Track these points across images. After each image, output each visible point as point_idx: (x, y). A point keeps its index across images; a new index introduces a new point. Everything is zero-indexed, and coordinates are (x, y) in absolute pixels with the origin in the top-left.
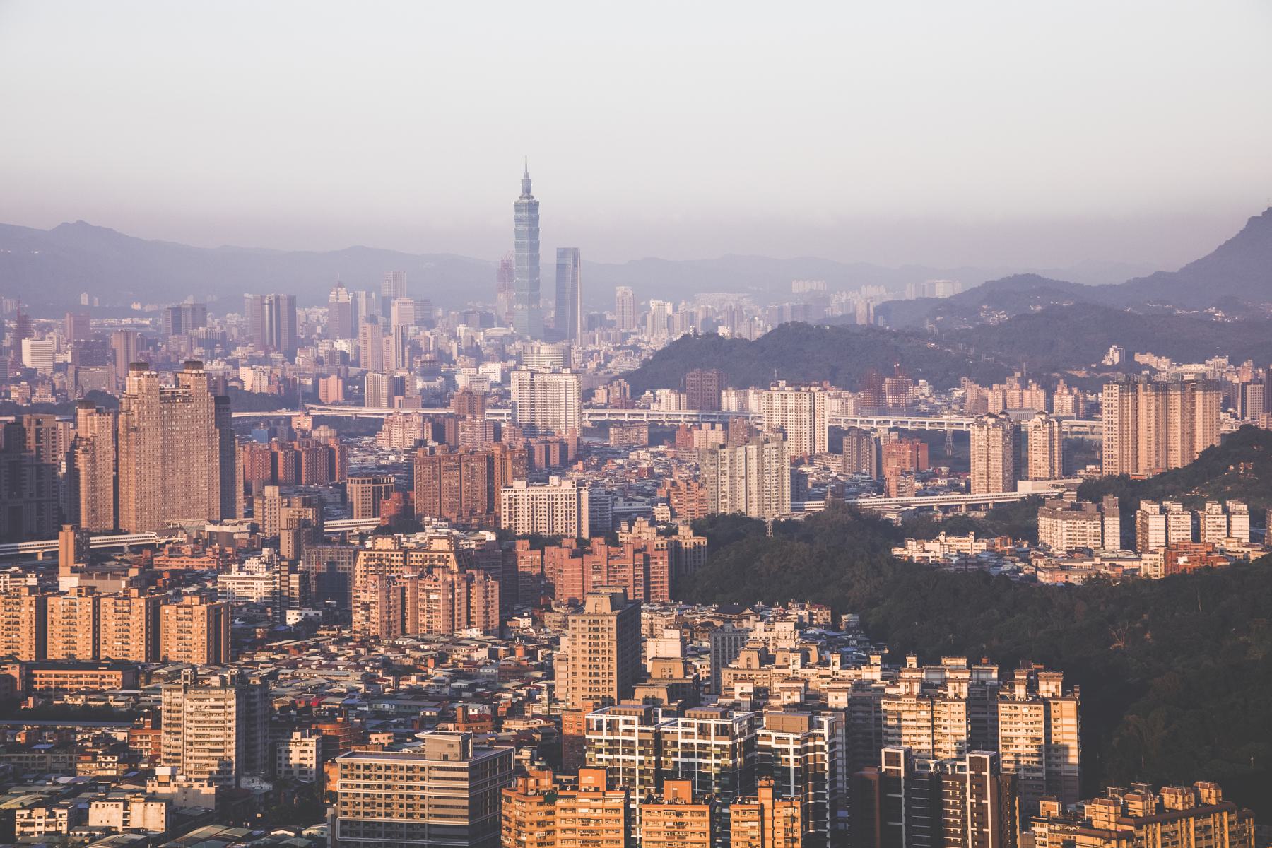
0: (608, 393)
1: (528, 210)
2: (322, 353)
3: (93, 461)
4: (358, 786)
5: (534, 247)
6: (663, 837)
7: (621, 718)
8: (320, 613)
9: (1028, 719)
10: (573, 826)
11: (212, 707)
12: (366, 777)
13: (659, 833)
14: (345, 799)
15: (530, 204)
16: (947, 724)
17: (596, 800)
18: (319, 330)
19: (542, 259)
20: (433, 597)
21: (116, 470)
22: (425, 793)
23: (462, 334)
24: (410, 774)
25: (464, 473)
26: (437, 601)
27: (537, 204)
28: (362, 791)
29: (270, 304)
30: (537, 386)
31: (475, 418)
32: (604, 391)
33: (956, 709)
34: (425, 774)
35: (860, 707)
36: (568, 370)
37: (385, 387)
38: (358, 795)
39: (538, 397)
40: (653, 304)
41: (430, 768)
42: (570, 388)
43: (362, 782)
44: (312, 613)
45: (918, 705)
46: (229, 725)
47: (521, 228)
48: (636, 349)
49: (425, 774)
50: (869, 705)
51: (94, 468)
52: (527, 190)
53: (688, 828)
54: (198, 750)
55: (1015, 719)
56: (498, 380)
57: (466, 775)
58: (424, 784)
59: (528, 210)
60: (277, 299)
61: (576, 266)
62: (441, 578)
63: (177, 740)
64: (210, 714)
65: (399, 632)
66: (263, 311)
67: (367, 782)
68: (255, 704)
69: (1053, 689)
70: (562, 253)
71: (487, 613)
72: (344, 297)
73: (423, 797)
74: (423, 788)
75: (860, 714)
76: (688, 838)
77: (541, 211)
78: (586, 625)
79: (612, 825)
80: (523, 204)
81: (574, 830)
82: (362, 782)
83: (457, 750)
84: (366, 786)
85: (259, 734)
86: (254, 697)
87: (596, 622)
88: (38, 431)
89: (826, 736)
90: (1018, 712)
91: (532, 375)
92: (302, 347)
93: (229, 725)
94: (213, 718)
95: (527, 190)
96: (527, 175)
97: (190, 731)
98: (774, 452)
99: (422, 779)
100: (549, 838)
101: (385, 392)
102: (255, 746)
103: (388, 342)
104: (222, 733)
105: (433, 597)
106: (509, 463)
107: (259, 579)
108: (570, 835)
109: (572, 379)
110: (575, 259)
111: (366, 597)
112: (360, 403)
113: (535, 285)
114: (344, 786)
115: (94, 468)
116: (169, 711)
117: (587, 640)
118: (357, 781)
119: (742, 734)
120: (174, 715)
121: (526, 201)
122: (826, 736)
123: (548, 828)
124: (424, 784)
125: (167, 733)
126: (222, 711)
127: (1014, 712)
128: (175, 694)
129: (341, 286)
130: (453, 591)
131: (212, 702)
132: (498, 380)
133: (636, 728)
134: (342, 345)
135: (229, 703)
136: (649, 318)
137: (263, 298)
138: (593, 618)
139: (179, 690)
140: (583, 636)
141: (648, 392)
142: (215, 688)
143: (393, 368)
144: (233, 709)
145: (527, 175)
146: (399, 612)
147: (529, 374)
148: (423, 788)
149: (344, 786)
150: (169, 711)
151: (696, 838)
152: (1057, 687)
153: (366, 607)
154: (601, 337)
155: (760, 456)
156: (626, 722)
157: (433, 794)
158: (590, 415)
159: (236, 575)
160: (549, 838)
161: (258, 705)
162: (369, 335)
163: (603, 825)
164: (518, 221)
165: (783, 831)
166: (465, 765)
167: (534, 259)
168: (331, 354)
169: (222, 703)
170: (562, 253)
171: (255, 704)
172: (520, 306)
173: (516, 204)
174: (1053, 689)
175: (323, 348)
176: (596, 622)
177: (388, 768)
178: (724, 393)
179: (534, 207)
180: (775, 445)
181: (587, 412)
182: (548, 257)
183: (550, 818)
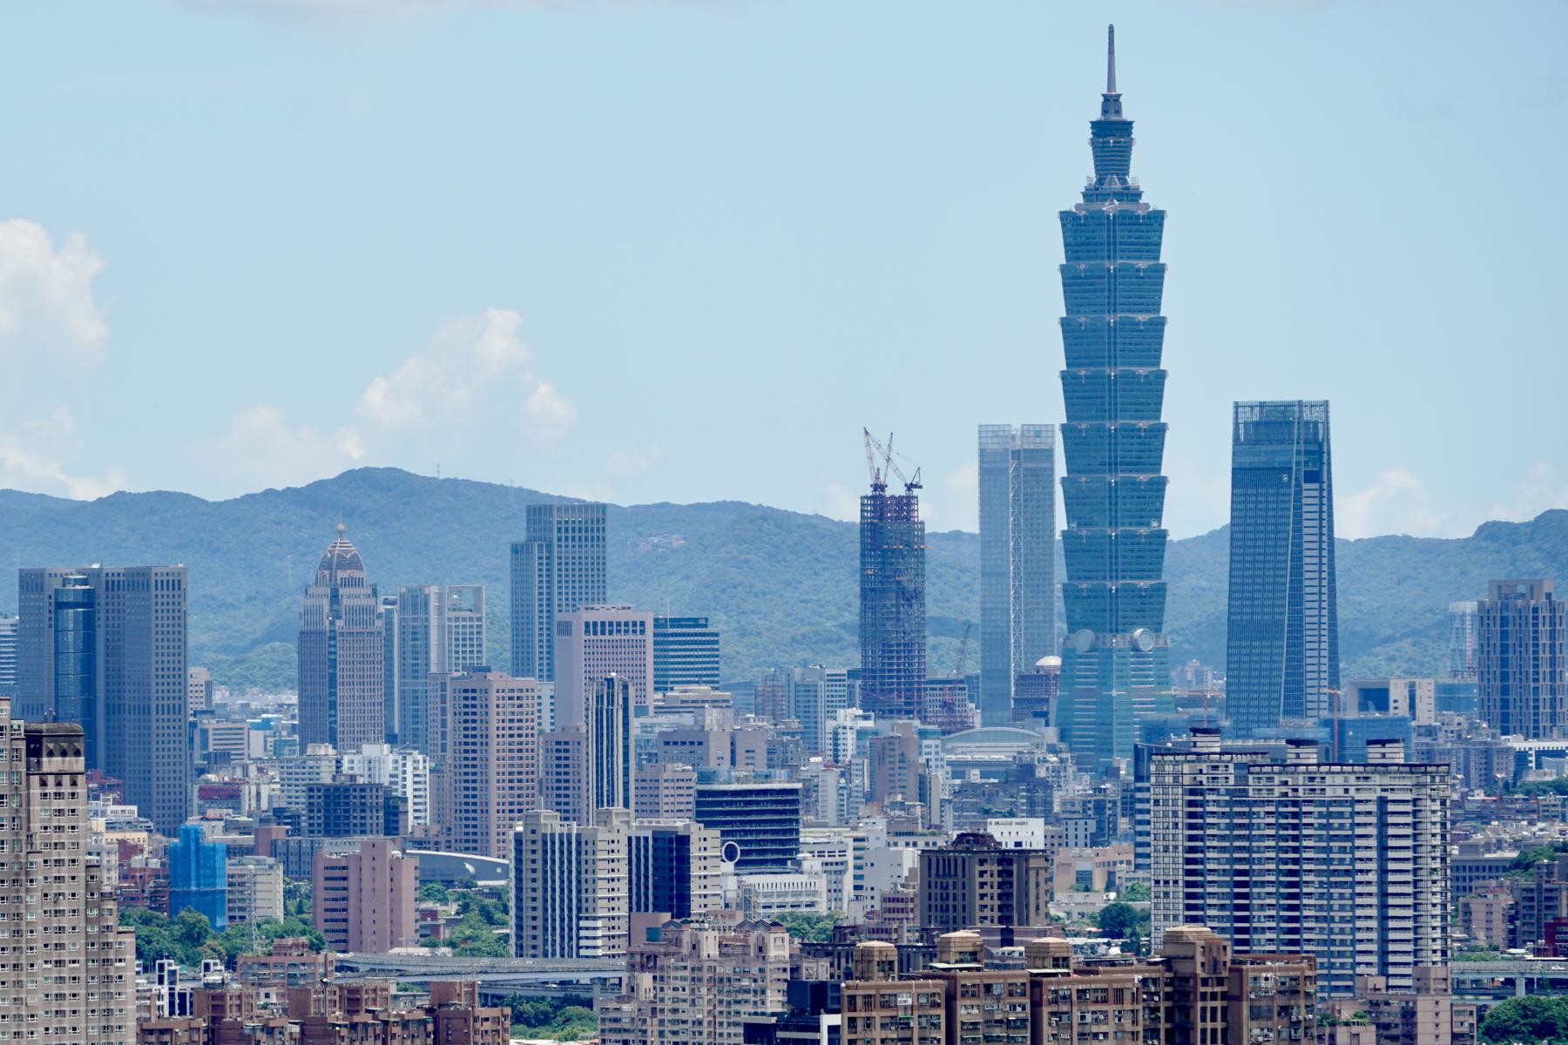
52: (1112, 136)
95: (1112, 136)
96: (1111, 102)
145: (1111, 102)
182: (1197, 496)
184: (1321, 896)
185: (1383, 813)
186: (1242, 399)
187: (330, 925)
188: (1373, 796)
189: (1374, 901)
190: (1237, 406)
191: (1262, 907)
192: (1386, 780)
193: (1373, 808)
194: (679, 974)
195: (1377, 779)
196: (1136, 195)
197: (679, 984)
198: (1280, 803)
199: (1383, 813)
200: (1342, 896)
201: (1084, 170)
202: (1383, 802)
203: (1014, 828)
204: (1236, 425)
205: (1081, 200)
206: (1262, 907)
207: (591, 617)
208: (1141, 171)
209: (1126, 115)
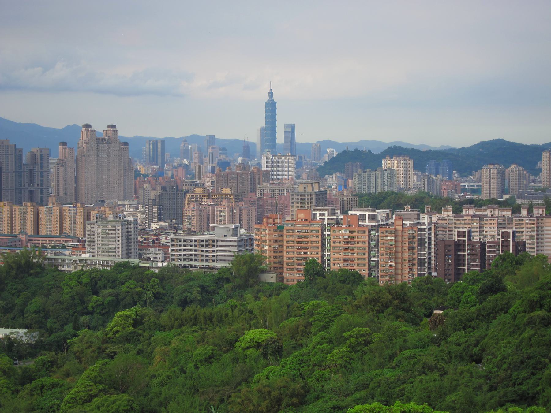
1: (271, 107)
3: (66, 170)
4: (180, 250)
6: (342, 245)
7: (318, 212)
8: (167, 224)
9: (529, 226)
10: (292, 250)
11: (110, 230)
12: (184, 246)
13: (340, 242)
14: (173, 257)
16: (487, 229)
17: (306, 225)
19: (277, 124)
20: (222, 214)
21: (76, 182)
22: (215, 254)
24: (207, 244)
25: (239, 181)
26: (224, 216)
27: (276, 103)
28: (182, 253)
29: (153, 144)
30: (275, 162)
33: (492, 222)
34: (215, 244)
35: (442, 229)
38: (180, 255)
41: (217, 241)
42: (290, 163)
43: (182, 248)
44: (163, 224)
45: (472, 220)
46: (118, 239)
49: (215, 244)
50: (445, 228)
51: (66, 174)
52: (271, 94)
53: (356, 239)
54: (103, 252)
55: (522, 226)
57: (236, 244)
58: (215, 249)
59: (271, 107)
62: (226, 205)
63: (93, 249)
64: (110, 234)
65: (205, 229)
67: (185, 248)
68: (131, 232)
69: (540, 212)
70: (287, 126)
71: (249, 223)
73: (214, 256)
74: (213, 251)
75: (441, 232)
76: (356, 245)
77: (277, 106)
78: (299, 197)
79: (314, 239)
81: (293, 252)
82: (182, 248)
83: (232, 232)
84: (185, 250)
85: (133, 247)
86: (130, 228)
87: (304, 195)
88: (41, 155)
89: (427, 223)
90: (523, 222)
91: (272, 157)
93: (118, 239)
94: (110, 236)
95: (271, 94)
96: (271, 90)
97: (98, 242)
98: (389, 175)
99: (214, 246)
100: (280, 249)
102: (131, 239)
104: (114, 243)
105: (222, 214)
106: (261, 176)
107: (140, 212)
108: (291, 244)
111: (189, 214)
114: (173, 250)
115: (66, 174)
116: (89, 235)
117: (299, 205)
118: (180, 248)
119: (382, 220)
120: (91, 237)
122: (427, 223)
123: (280, 243)
124: (215, 249)
125: (88, 245)
126: (114, 232)
127: (521, 222)
128: (92, 226)
130: (233, 210)
131: (110, 228)
133: (326, 217)
134: (185, 161)
135: (118, 228)
138: (302, 194)
139: (94, 224)
140: (298, 203)
142: (111, 221)
144: (120, 231)
145: (271, 90)
146: (205, 221)
147: (271, 157)
148: (213, 251)
149: (173, 250)
150: (89, 235)
151: (360, 245)
152: (543, 211)
153: (189, 218)
155: (383, 178)
156: (320, 214)
157: (219, 254)
159: (128, 210)
160: (280, 249)
161: (132, 233)
163: (310, 239)
165: (407, 243)
166: (236, 239)
168: (181, 165)
169: (114, 228)
171: (131, 232)
173: (266, 103)
174: (540, 212)
176: (304, 195)
177: (196, 241)
180: (389, 172)
183: (280, 238)
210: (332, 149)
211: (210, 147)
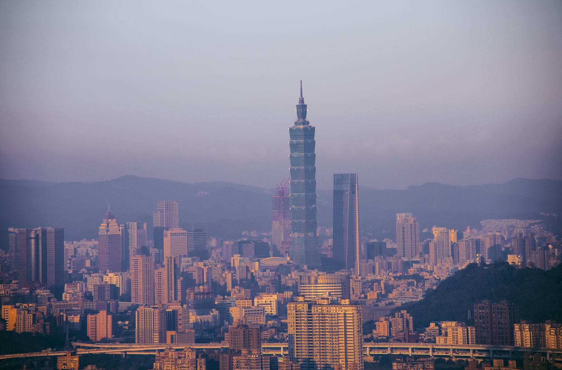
0: (390, 326)
1: (304, 137)
2: (91, 288)
5: (310, 173)
15: (305, 129)
18: (88, 263)
23: (237, 264)
27: (313, 129)
29: (37, 238)
30: (315, 317)
31: (250, 353)
32: (386, 323)
36: (347, 301)
37: (157, 322)
39: (316, 329)
40: (436, 231)
42: (349, 320)
47: (295, 155)
48: (418, 278)
52: (302, 109)
56: (274, 313)
59: (304, 137)
60: (44, 232)
61: (354, 192)
66: (28, 245)
70: (339, 179)
72: (115, 228)
77: (317, 137)
80: (299, 130)
91: (310, 307)
92: (70, 282)
95: (302, 109)
96: (302, 101)
101: (157, 327)
103: (160, 274)
109: (351, 310)
110: (353, 186)
112: (131, 341)
113: (311, 214)
121: (302, 127)
129: (111, 217)
132: (274, 313)
136: (431, 245)
137: (29, 232)
141: (432, 325)
143: (165, 302)
145: (302, 101)
147: (306, 306)
154: (381, 267)
158: (371, 349)
162: (140, 267)
164: (293, 147)
167: (311, 186)
170: (339, 179)
172: (296, 235)
173: (291, 130)
175: (92, 281)
178: (517, 327)
179: (309, 133)
181: (368, 346)
184: (330, 338)
185: (345, 317)
186: (335, 173)
187: (92, 333)
188: (343, 313)
189: (343, 336)
190: (334, 175)
191: (315, 341)
192: (346, 308)
193: (343, 315)
194: (168, 363)
195: (343, 308)
196: (308, 123)
197: (168, 365)
198: (319, 314)
199: (345, 317)
200: (335, 338)
201: (295, 118)
202: (345, 314)
203: (270, 298)
204: (334, 179)
205: (294, 125)
206: (315, 341)
207: (172, 232)
208: (308, 118)
209: (305, 103)
210: (441, 229)
211: (169, 232)
